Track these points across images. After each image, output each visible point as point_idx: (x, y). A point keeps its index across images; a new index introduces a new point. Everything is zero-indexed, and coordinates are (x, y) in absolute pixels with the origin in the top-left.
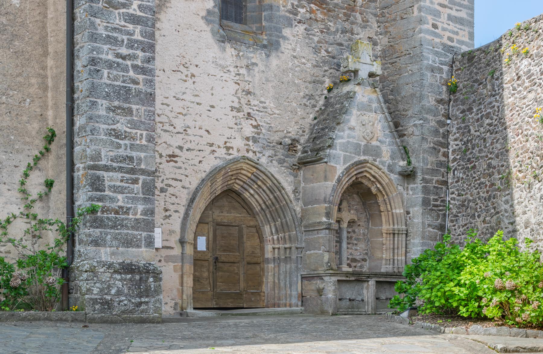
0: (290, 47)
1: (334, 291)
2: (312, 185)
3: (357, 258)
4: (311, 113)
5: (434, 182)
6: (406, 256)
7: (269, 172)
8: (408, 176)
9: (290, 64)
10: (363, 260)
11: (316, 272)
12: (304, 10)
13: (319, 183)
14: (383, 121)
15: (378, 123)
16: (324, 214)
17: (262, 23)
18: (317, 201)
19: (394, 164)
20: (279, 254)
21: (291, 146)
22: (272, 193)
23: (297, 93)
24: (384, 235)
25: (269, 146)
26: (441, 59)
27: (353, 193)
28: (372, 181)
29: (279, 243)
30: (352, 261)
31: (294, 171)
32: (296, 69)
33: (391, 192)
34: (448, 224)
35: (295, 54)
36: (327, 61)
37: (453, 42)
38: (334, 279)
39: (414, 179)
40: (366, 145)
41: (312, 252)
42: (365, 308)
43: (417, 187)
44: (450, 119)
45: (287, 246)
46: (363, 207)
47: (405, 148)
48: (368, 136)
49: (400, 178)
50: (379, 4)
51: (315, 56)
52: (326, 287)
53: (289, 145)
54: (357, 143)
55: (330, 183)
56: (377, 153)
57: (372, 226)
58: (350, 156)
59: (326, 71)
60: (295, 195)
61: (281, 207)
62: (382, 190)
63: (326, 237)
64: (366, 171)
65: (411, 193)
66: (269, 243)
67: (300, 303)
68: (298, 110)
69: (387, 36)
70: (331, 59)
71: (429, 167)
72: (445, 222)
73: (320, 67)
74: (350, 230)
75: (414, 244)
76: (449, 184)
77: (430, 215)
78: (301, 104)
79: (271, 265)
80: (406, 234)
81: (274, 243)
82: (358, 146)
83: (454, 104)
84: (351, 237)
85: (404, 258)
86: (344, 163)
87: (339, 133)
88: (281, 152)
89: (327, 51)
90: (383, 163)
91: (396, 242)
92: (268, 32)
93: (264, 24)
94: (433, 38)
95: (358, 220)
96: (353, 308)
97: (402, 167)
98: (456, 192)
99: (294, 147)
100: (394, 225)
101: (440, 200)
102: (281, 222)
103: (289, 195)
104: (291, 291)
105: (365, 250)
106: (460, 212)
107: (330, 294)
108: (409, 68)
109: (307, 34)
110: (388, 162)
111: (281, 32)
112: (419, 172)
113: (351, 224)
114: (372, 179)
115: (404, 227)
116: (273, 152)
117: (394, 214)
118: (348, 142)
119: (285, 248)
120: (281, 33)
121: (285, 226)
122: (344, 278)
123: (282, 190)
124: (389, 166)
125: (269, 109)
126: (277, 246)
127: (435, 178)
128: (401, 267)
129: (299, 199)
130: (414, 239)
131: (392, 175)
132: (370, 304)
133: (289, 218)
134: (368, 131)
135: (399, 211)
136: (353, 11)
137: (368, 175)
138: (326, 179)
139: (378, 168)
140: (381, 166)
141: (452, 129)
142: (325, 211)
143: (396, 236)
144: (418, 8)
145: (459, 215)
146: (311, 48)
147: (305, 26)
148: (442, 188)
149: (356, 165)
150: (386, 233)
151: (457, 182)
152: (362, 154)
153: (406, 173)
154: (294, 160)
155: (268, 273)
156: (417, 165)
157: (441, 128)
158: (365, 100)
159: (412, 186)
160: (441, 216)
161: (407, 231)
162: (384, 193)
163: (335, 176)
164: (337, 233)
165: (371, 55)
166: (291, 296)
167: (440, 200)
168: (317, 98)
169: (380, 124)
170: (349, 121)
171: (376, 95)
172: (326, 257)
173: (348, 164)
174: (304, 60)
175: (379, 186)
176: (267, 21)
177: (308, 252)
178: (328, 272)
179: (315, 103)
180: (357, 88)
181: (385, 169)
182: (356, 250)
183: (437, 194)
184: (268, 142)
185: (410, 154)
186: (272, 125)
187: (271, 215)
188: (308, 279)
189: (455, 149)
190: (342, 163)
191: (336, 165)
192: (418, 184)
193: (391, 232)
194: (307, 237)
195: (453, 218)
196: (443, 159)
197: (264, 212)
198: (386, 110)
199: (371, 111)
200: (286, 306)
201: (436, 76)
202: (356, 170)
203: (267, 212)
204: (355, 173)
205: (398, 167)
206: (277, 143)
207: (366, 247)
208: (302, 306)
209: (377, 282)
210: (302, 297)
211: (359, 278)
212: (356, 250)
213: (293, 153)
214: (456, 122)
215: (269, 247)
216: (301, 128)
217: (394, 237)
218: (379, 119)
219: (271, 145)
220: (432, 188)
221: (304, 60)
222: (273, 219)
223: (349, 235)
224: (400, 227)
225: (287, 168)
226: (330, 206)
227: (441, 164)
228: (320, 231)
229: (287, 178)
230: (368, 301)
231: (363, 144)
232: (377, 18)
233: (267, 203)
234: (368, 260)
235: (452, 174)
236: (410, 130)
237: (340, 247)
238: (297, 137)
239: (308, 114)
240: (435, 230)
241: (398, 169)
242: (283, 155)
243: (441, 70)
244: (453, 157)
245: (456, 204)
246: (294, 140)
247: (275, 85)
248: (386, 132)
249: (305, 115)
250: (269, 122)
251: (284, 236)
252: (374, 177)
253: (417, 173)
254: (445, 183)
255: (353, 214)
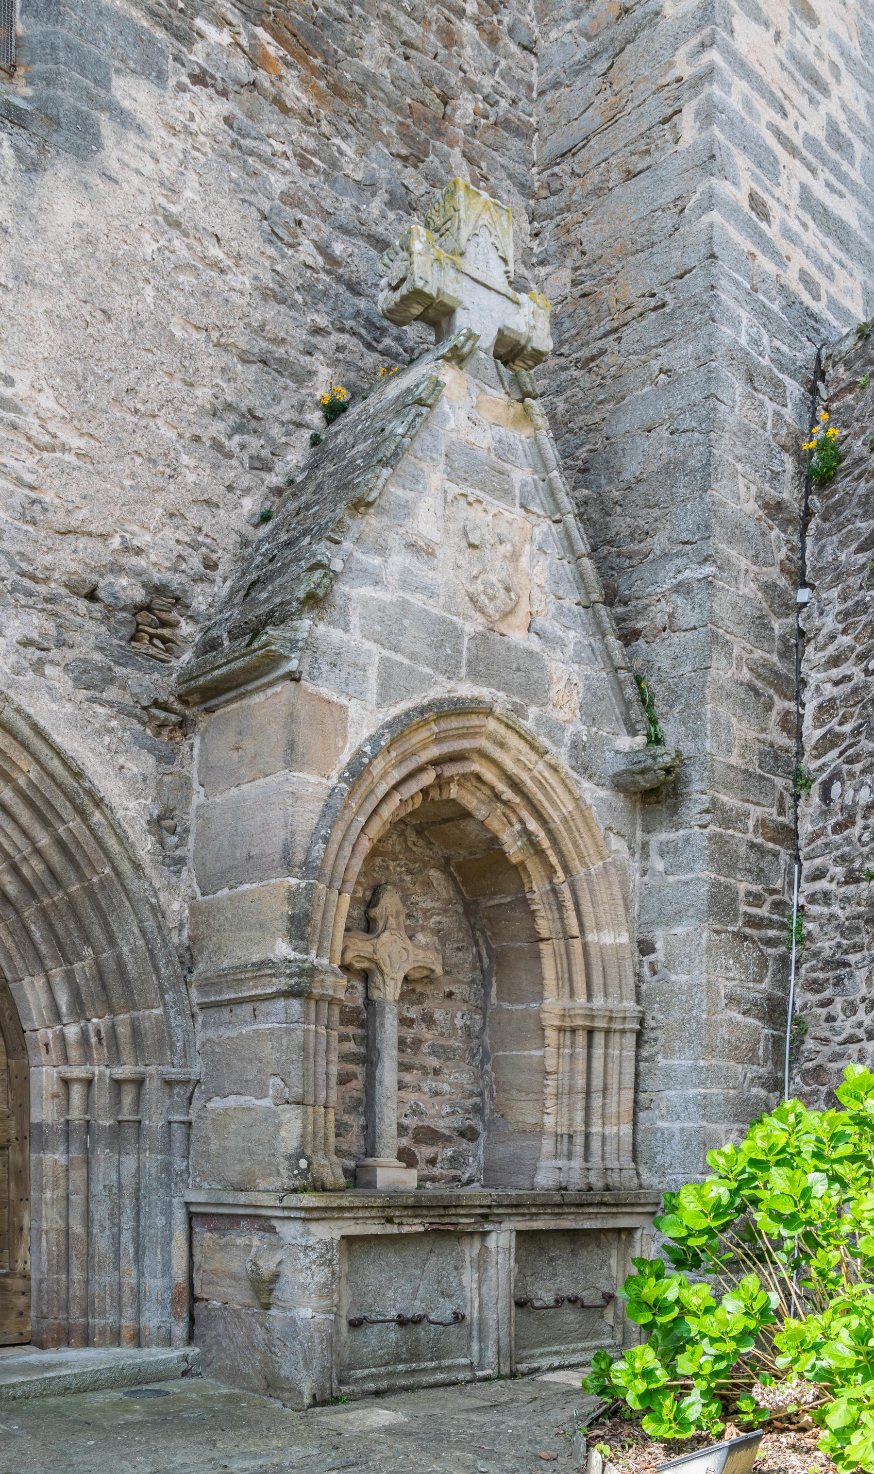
0: (149, 168)
1: (326, 1290)
2: (234, 791)
3: (442, 1125)
4: (247, 491)
5: (751, 823)
6: (635, 1123)
7: (19, 710)
8: (654, 793)
9: (149, 248)
10: (462, 1134)
11: (242, 1198)
12: (225, 38)
13: (261, 782)
14: (554, 551)
15: (532, 556)
16: (283, 925)
17: (11, 23)
18: (252, 866)
19: (598, 742)
20: (88, 1107)
21: (143, 616)
22: (46, 824)
23: (177, 384)
24: (551, 1035)
25: (30, 594)
26: (777, 343)
27: (426, 865)
28: (506, 803)
29: (87, 1058)
30: (417, 1140)
31: (158, 734)
32: (181, 278)
33: (581, 857)
34: (798, 997)
35: (174, 209)
36: (325, 294)
37: (817, 297)
38: (328, 1232)
39: (674, 810)
40: (479, 638)
41: (232, 1101)
42: (468, 1353)
43: (687, 840)
44: (804, 585)
45: (124, 1071)
46: (465, 924)
47: (638, 680)
48: (492, 599)
49: (619, 801)
50: (540, 148)
51: (271, 251)
52: (286, 1270)
53: (139, 609)
54: (443, 621)
55: (313, 779)
56: (529, 683)
57: (500, 998)
58: (411, 671)
59: (317, 331)
60: (162, 843)
61: (89, 892)
62: (546, 844)
63: (289, 1031)
64: (483, 754)
65: (659, 865)
66: (44, 1058)
67: (180, 1330)
68: (185, 459)
69: (569, 262)
70: (342, 289)
71: (734, 760)
72: (785, 988)
73: (293, 306)
74: (413, 1013)
75: (668, 1073)
76: (801, 842)
77: (737, 958)
78: (197, 439)
79: (54, 1158)
80: (639, 1034)
81: (66, 1060)
82: (445, 634)
83: (827, 525)
84: (417, 1042)
85: (626, 1129)
86: (385, 697)
87: (358, 555)
88: (90, 636)
89: (323, 249)
90: (554, 729)
91: (598, 1065)
92: (38, 67)
93: (20, 28)
94: (753, 249)
95: (446, 973)
96: (414, 1356)
97: (626, 754)
98: (839, 871)
99: (164, 624)
100: (590, 997)
101: (770, 899)
102: (98, 963)
103: (132, 837)
104: (141, 1274)
105: (472, 1094)
106: (857, 948)
107: (306, 1305)
108: (655, 365)
109: (234, 144)
110: (571, 729)
111: (104, 83)
112: (695, 776)
113: (419, 988)
114: (508, 794)
115: (630, 1004)
116: (53, 631)
117: (593, 951)
118: (404, 606)
119: (118, 1083)
120: (108, 89)
121: (111, 980)
122: (374, 1228)
123: (91, 807)
124: (574, 746)
125: (32, 419)
126: (77, 1072)
127: (756, 812)
128: (615, 1165)
129: (181, 861)
130: (669, 1053)
131: (586, 784)
132: (492, 1336)
133: (131, 941)
134: (493, 578)
135: (611, 938)
136: (439, 134)
137: (490, 775)
138: (292, 755)
139: (533, 747)
140: (544, 741)
141: (817, 623)
142: (287, 909)
143: (599, 1039)
144: (697, 114)
145: (852, 958)
146: (256, 215)
147: (225, 107)
148: (776, 855)
149: (440, 717)
150: (561, 1029)
151: (838, 828)
152: (463, 671)
153: (644, 782)
154: (161, 683)
155: (41, 1189)
156: (688, 748)
157: (779, 616)
158: (483, 439)
159: (663, 836)
160: (772, 966)
161: (642, 1021)
162: (554, 860)
163: (339, 750)
164: (349, 1017)
165: (510, 256)
166: (138, 1294)
167: (770, 899)
168: (276, 431)
169: (543, 562)
170: (406, 510)
171: (529, 431)
172: (291, 1128)
173: (404, 706)
174: (215, 251)
175: (533, 825)
176: (36, 15)
177: (216, 1103)
178: (293, 1200)
179: (265, 453)
180: (449, 375)
181: (562, 756)
182: (437, 1094)
183: (759, 875)
184: (23, 574)
185: (660, 707)
186: (48, 497)
187: (51, 927)
188: (216, 1222)
189: (832, 700)
190: (372, 696)
191: (343, 700)
192: (694, 829)
193: (579, 1022)
194: (210, 1034)
195: (821, 975)
196: (783, 740)
197: (17, 912)
198: (567, 504)
199: (505, 493)
200: (116, 1339)
201: (762, 404)
202: (439, 739)
203: (29, 912)
204: (434, 752)
205: (609, 755)
206: (72, 588)
207: (476, 1081)
208: (191, 1338)
209: (519, 1233)
210: (190, 1302)
211: (443, 1223)
212: (437, 1094)
213: (153, 651)
214: (835, 593)
215: (45, 1076)
216: (195, 546)
217: (590, 1046)
218: (538, 537)
219: (42, 589)
220: (743, 850)
221: (215, 251)
222: (60, 946)
223: (410, 1034)
224: (613, 1003)
225: (123, 711)
226: (310, 888)
227: (776, 758)
228: (263, 1007)
229: (121, 760)
230: (481, 1320)
231: (469, 628)
232: (532, 202)
233: (25, 871)
234: (484, 1134)
235: (816, 800)
236: (659, 613)
237: (370, 1082)
238: (175, 580)
239: (230, 488)
240: (751, 1020)
241: (612, 765)
242: (101, 649)
243: (778, 391)
244: (819, 733)
245: (832, 916)
246: (159, 590)
247: (65, 313)
248: (566, 603)
249: (216, 491)
250: (29, 478)
251: (113, 1028)
252: (515, 785)
253: (687, 784)
254: (788, 835)
255: (426, 947)
